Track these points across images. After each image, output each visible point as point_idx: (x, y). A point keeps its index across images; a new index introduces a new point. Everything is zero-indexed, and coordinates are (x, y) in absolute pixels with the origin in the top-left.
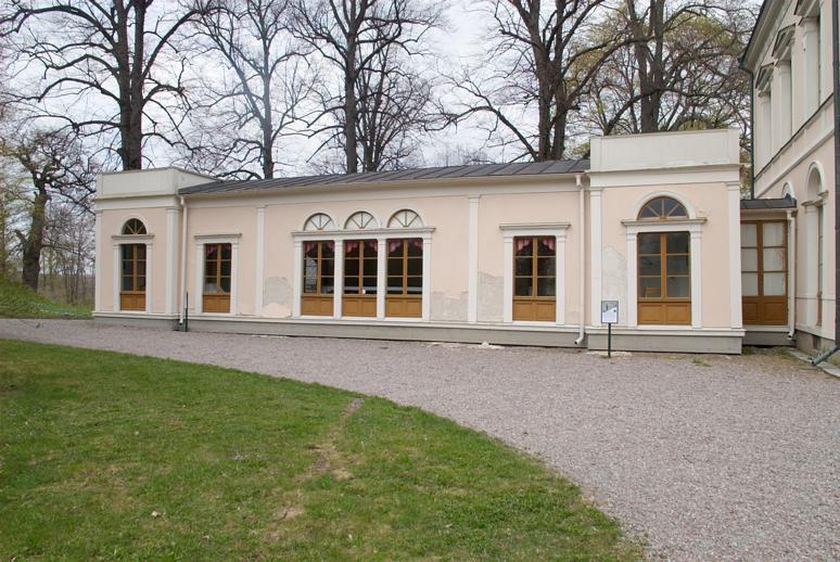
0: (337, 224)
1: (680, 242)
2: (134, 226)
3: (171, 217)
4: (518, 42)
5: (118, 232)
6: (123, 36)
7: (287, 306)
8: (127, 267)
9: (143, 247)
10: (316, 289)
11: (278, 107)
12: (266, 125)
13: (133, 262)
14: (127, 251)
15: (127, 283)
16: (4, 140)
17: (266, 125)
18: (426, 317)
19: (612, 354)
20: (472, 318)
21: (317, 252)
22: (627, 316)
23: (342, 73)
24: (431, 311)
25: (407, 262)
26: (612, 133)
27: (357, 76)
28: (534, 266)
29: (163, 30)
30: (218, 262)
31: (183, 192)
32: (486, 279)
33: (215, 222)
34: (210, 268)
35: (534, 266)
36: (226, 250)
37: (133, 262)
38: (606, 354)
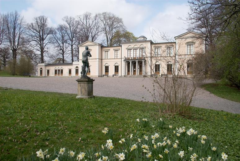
0: (60, 68)
1: (78, 69)
2: (41, 68)
4: (191, 49)
5: (75, 67)
7: (54, 75)
8: (41, 72)
10: (56, 73)
11: (65, 49)
12: (63, 51)
13: (41, 71)
14: (41, 70)
15: (41, 73)
16: (1, 49)
17: (63, 51)
18: (91, 75)
21: (56, 71)
22: (75, 75)
25: (62, 71)
28: (70, 71)
30: (48, 71)
32: (67, 72)
33: (48, 68)
34: (48, 72)
35: (70, 71)
36: (71, 70)
37: (41, 71)
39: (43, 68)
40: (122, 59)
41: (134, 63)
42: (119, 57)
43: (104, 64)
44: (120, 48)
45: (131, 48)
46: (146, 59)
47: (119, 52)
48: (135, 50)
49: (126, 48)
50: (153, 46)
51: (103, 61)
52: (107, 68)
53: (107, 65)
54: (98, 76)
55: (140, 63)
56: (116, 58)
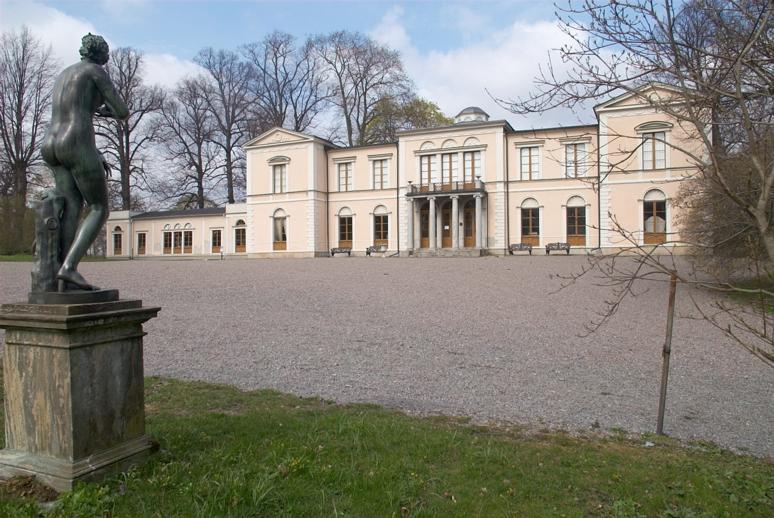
3: (128, 225)
5: (234, 224)
6: (121, 143)
7: (160, 252)
8: (116, 241)
9: (244, 230)
13: (118, 239)
14: (238, 231)
15: (116, 246)
19: (571, 252)
20: (203, 253)
21: (167, 236)
23: (446, 116)
24: (195, 251)
25: (189, 236)
26: (56, 207)
27: (362, 129)
29: (139, 141)
30: (142, 238)
31: (132, 217)
33: (141, 226)
36: (219, 232)
37: (118, 239)
38: (565, 252)
39: (126, 227)
40: (401, 191)
41: (444, 206)
42: (390, 183)
43: (334, 209)
44: (393, 150)
45: (477, 147)
46: (488, 189)
47: (390, 166)
48: (469, 157)
49: (416, 152)
50: (512, 140)
51: (332, 198)
52: (346, 225)
53: (345, 213)
54: (313, 255)
55: (467, 205)
56: (378, 187)
